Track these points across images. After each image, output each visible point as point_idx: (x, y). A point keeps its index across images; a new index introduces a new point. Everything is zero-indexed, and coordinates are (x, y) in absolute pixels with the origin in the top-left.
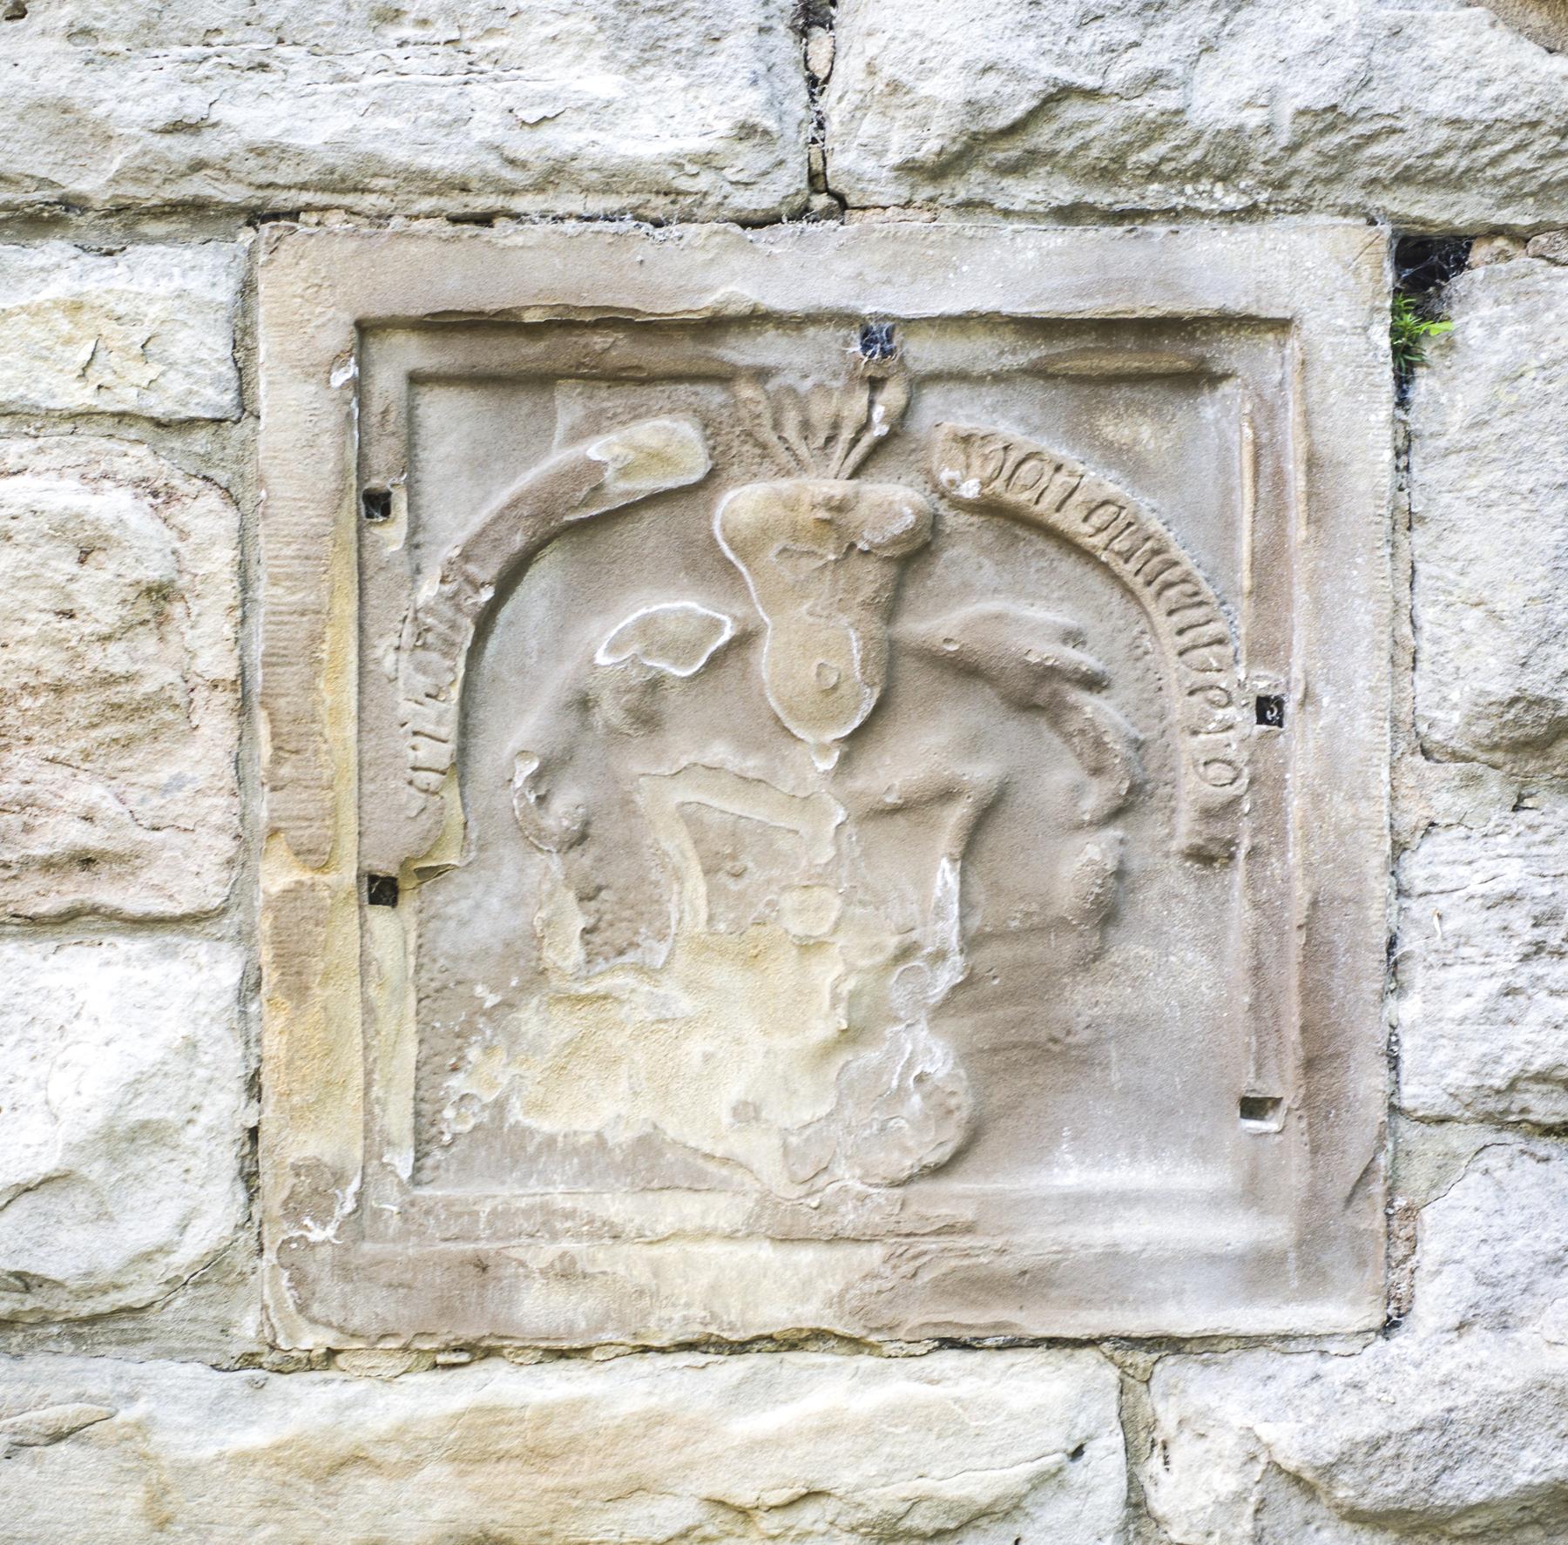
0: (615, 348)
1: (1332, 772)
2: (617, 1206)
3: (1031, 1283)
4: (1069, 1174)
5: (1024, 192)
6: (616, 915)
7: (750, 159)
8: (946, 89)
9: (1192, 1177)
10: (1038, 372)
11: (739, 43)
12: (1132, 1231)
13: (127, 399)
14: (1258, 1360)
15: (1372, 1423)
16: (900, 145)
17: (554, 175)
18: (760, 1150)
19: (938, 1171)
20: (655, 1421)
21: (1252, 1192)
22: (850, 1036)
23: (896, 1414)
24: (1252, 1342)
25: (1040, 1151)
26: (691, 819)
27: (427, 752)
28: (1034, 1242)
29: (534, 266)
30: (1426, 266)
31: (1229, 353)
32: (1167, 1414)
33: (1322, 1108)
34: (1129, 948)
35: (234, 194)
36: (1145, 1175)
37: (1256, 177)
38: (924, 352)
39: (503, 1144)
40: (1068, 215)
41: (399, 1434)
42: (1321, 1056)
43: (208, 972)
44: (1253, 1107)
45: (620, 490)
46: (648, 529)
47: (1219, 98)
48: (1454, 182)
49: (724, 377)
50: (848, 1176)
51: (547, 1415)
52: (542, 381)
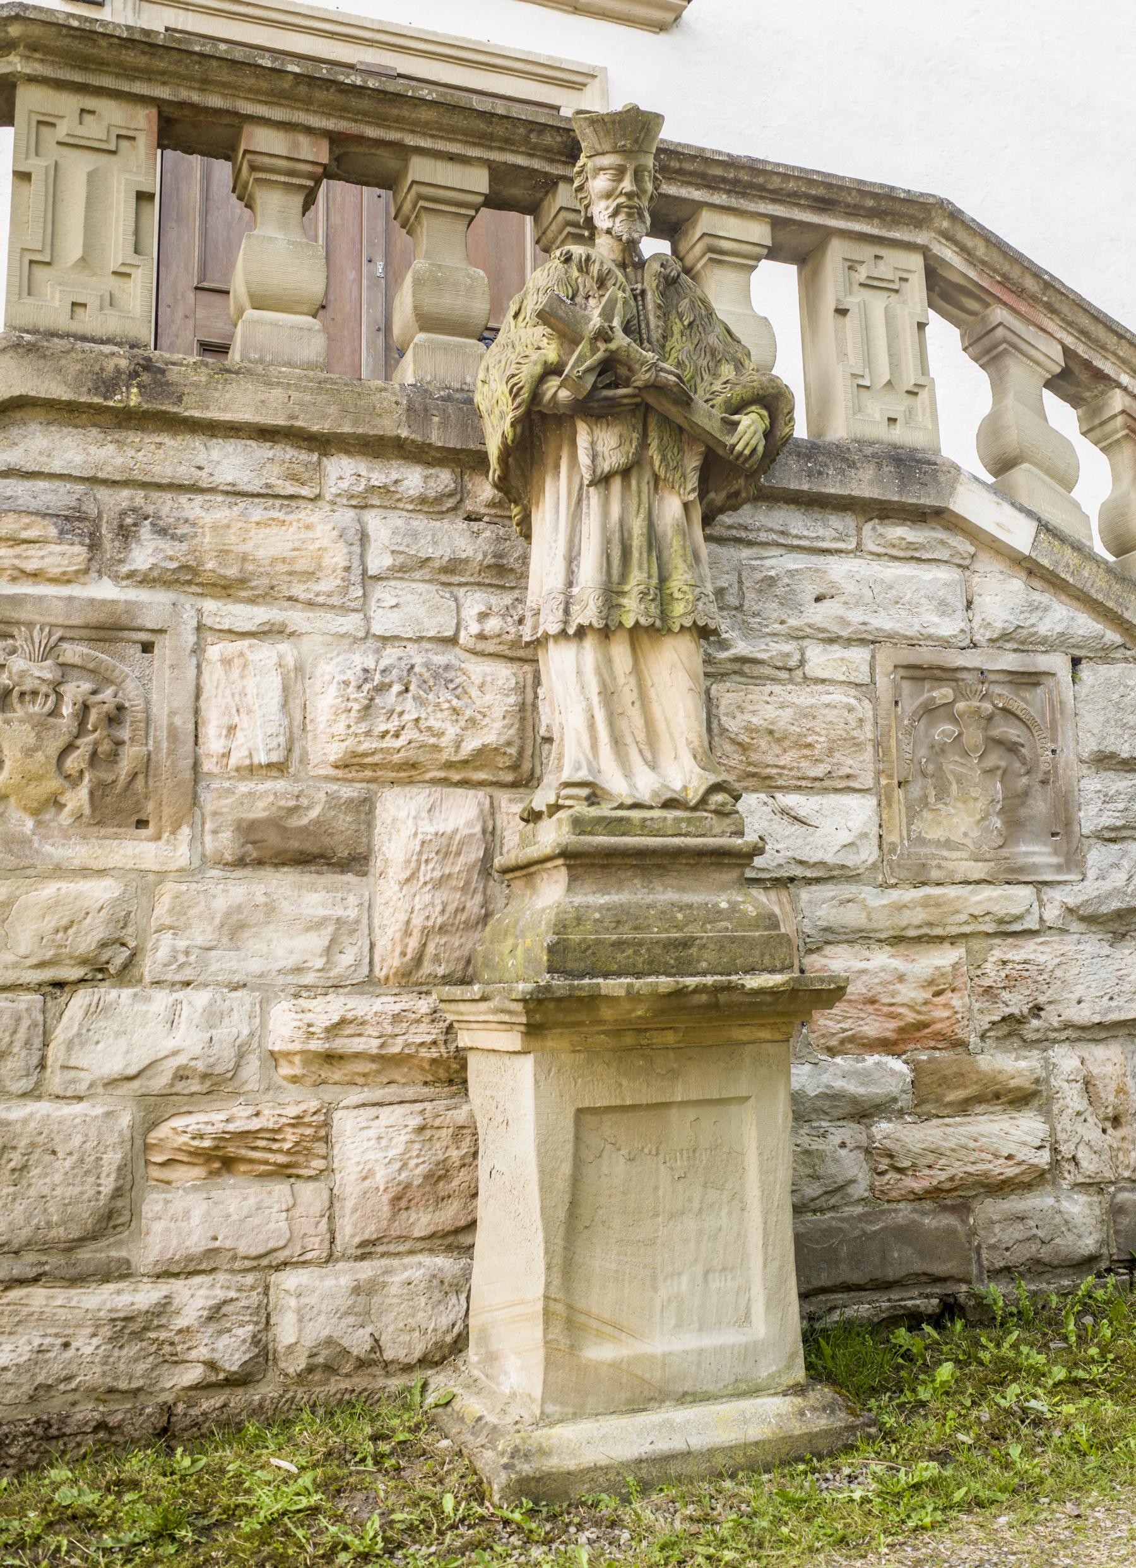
0: (937, 673)
1: (1067, 765)
2: (945, 853)
3: (1021, 870)
4: (1023, 848)
5: (1008, 646)
6: (942, 792)
7: (962, 636)
8: (999, 625)
9: (1045, 849)
10: (1010, 682)
11: (959, 613)
12: (1036, 859)
13: (852, 679)
14: (1061, 887)
15: (1086, 897)
16: (988, 635)
17: (929, 637)
18: (968, 841)
19: (1000, 847)
20: (959, 898)
21: (1056, 853)
22: (983, 819)
23: (1001, 896)
24: (1059, 883)
25: (1017, 844)
26: (952, 772)
27: (908, 756)
28: (1021, 861)
29: (925, 655)
30: (1076, 662)
31: (1043, 679)
32: (1045, 898)
33: (1068, 834)
34: (1031, 801)
35: (871, 638)
36: (1036, 849)
37: (1049, 645)
38: (992, 677)
39: (921, 841)
40: (1015, 650)
41: (912, 901)
42: (1068, 824)
43: (871, 801)
44: (1053, 835)
45: (939, 702)
46: (941, 711)
47: (1043, 629)
48: (1081, 647)
49: (956, 680)
50: (985, 848)
51: (939, 896)
52: (923, 679)
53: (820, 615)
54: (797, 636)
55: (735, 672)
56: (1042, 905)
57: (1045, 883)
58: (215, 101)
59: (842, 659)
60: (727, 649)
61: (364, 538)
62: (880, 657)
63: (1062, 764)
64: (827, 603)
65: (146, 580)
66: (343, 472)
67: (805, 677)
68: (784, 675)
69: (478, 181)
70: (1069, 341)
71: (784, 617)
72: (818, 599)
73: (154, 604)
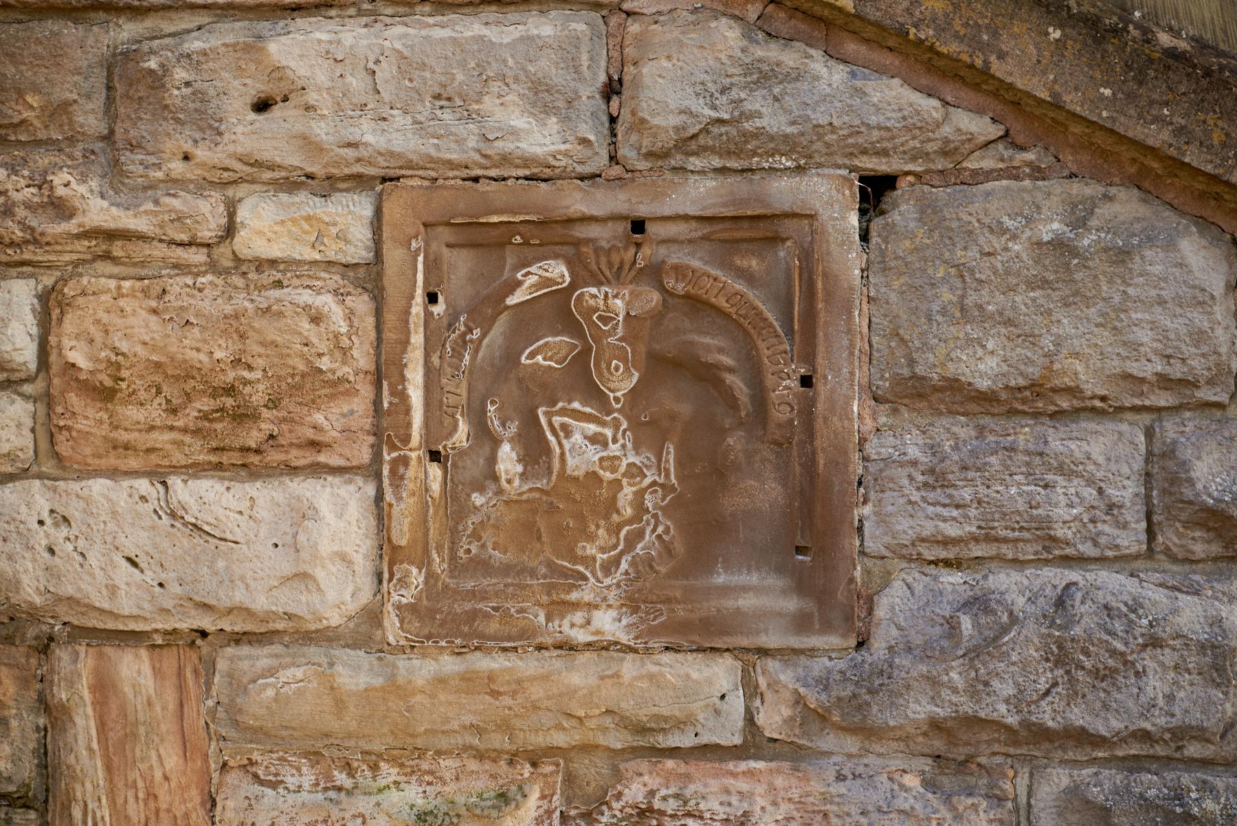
5: (695, 163)
12: (746, 602)
13: (331, 256)
28: (711, 606)
29: (502, 205)
30: (875, 191)
36: (754, 579)
37: (803, 152)
53: (269, 138)
54: (225, 182)
55: (96, 258)
56: (751, 691)
57: (763, 652)
59: (308, 218)
60: (71, 216)
62: (394, 209)
63: (821, 407)
64: (277, 112)
67: (237, 259)
68: (197, 257)
71: (188, 147)
72: (262, 106)
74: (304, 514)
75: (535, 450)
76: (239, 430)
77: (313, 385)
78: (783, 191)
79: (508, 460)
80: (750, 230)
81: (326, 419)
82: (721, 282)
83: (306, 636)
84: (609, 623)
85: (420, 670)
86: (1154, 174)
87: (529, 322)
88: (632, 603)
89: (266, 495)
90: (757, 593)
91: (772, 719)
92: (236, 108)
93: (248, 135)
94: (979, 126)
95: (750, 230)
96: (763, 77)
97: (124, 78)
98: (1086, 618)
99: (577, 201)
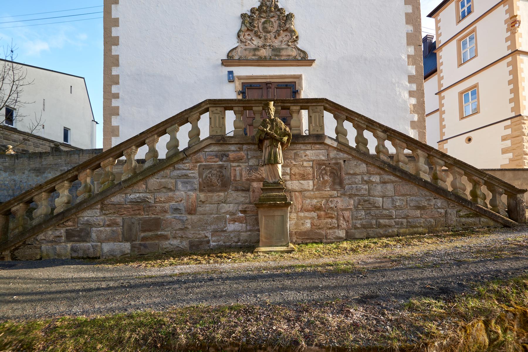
30: (344, 161)
37: (340, 159)
53: (306, 158)
54: (302, 161)
58: (230, 105)
61: (248, 154)
65: (224, 161)
66: (245, 147)
69: (261, 108)
70: (347, 115)
73: (225, 164)
74: (309, 183)
75: (323, 178)
76: (303, 177)
77: (309, 174)
78: (339, 161)
79: (321, 179)
80: (337, 164)
81: (310, 176)
82: (335, 167)
83: (308, 191)
84: (328, 189)
85: (316, 193)
86: (361, 160)
87: (322, 170)
88: (330, 188)
89: (306, 181)
90: (338, 187)
91: (339, 195)
92: (303, 156)
93: (304, 158)
94: (351, 157)
95: (337, 164)
96: (338, 154)
97: (296, 154)
98: (358, 187)
99: (326, 162)
